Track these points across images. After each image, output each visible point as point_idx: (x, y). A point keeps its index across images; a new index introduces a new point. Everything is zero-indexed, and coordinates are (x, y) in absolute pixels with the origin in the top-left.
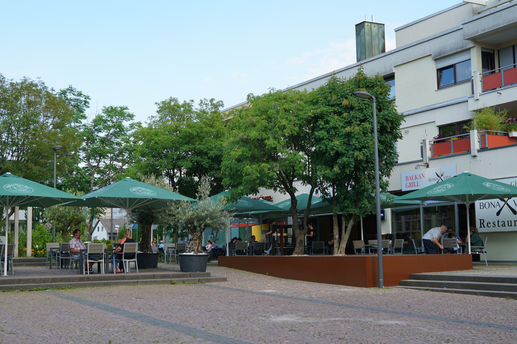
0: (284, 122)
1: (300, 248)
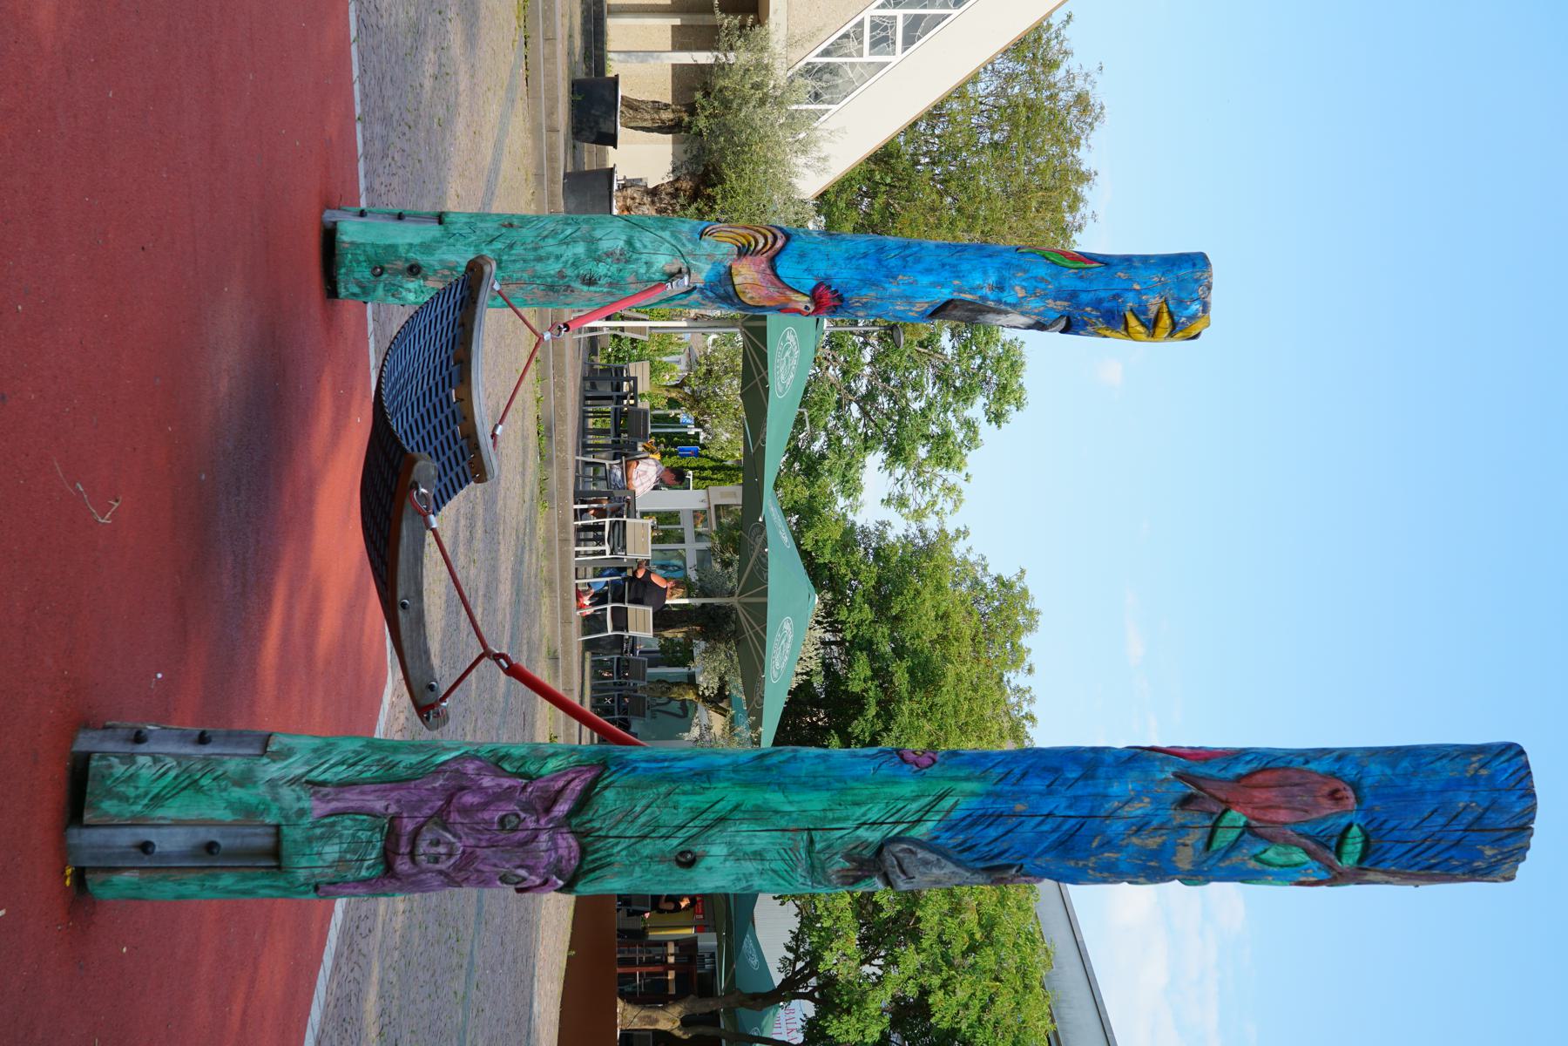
0: (962, 994)
1: (636, 1020)
